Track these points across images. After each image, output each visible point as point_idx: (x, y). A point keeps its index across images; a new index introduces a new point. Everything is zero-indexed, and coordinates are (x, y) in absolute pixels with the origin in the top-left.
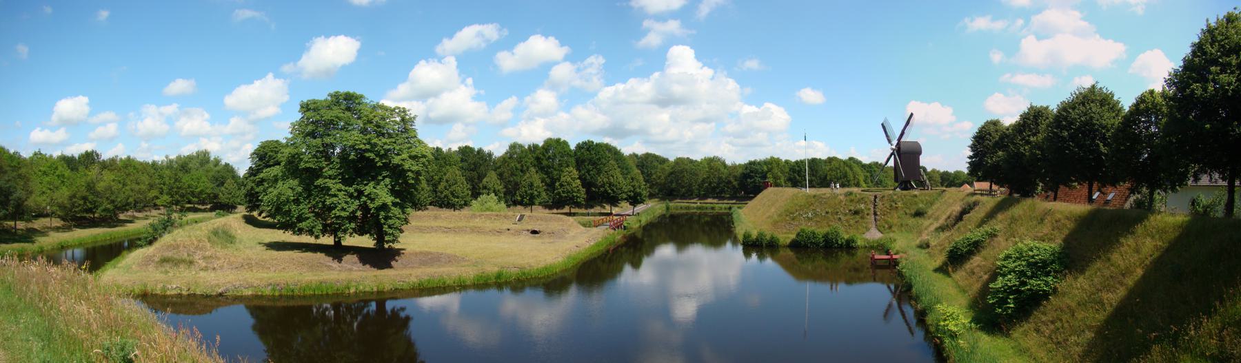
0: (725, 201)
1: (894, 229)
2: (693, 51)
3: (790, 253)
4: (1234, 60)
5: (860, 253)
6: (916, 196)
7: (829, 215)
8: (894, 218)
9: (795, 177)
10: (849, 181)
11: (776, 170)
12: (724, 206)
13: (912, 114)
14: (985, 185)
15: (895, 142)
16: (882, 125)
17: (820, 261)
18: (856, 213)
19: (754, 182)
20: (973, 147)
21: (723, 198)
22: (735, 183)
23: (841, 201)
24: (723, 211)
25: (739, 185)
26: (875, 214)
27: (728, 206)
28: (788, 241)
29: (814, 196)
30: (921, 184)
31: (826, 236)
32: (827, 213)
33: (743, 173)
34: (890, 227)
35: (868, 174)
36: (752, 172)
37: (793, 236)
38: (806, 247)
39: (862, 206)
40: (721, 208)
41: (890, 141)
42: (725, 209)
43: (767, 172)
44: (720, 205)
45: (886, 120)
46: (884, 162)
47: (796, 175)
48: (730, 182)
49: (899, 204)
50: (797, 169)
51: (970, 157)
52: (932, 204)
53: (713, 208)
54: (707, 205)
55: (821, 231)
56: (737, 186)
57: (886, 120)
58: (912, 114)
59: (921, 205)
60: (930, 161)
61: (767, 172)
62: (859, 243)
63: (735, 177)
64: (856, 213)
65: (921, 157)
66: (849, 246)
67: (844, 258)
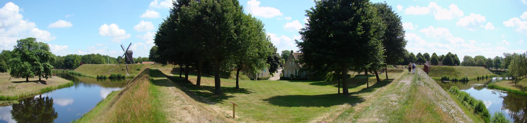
0: (60, 70)
1: (133, 73)
2: (18, 6)
3: (109, 80)
4: (107, 122)
5: (126, 79)
6: (136, 65)
7: (116, 70)
8: (132, 71)
9: (83, 61)
10: (101, 62)
11: (77, 59)
12: (61, 71)
13: (131, 43)
14: (153, 63)
15: (125, 51)
16: (121, 45)
17: (117, 82)
18: (123, 70)
19: (70, 63)
20: (150, 53)
21: (59, 69)
22: (63, 63)
23: (118, 67)
24: (61, 73)
25: (64, 64)
26: (127, 70)
27: (63, 71)
28: (108, 77)
29: (111, 66)
30: (133, 63)
31: (118, 75)
32: (115, 70)
33: (65, 60)
34: (132, 73)
35: (106, 60)
36: (69, 59)
37: (110, 76)
38: (113, 78)
39: (124, 68)
40: (60, 72)
41: (124, 50)
42: (61, 72)
43: (74, 60)
44: (60, 71)
45: (122, 44)
46: (337, 93)
47: (84, 60)
48: (61, 63)
49: (133, 67)
50: (84, 58)
51: (149, 55)
52: (141, 67)
53: (57, 72)
54: (55, 71)
55: (116, 74)
56: (64, 64)
57: (122, 44)
58: (131, 43)
59: (138, 68)
60: (135, 56)
61: (74, 60)
62: (126, 77)
63: (63, 61)
64: (123, 70)
65: (133, 55)
66: (124, 78)
67: (122, 80)
